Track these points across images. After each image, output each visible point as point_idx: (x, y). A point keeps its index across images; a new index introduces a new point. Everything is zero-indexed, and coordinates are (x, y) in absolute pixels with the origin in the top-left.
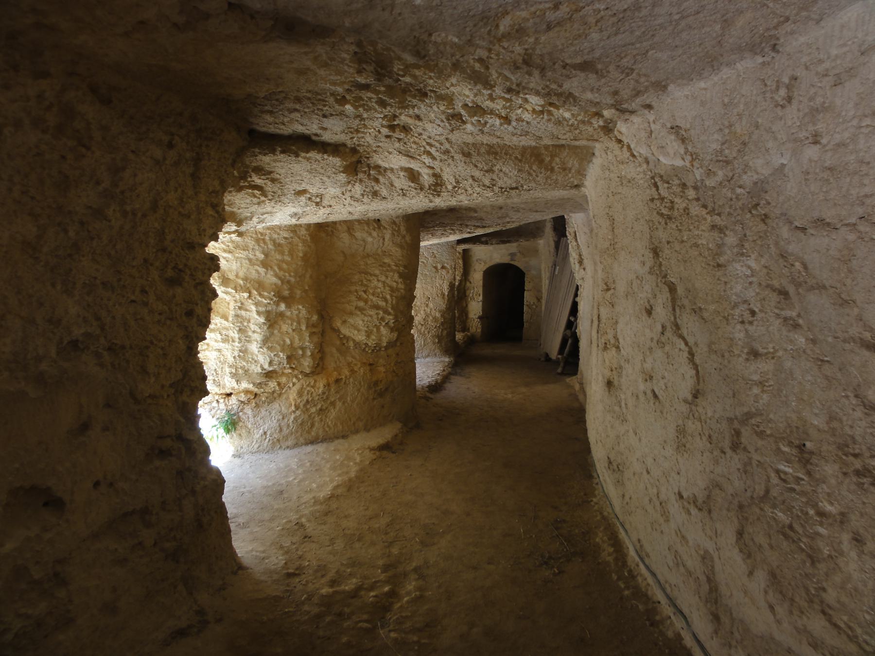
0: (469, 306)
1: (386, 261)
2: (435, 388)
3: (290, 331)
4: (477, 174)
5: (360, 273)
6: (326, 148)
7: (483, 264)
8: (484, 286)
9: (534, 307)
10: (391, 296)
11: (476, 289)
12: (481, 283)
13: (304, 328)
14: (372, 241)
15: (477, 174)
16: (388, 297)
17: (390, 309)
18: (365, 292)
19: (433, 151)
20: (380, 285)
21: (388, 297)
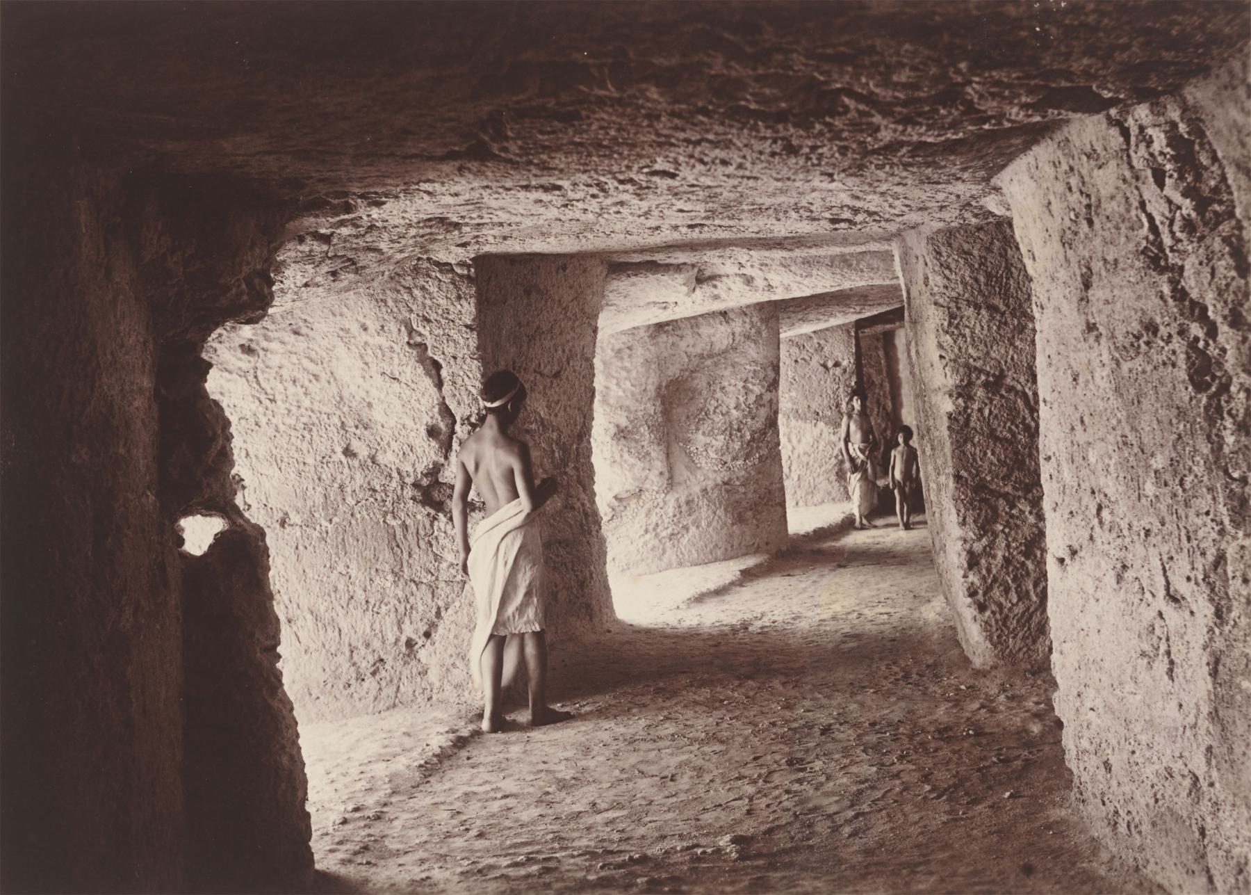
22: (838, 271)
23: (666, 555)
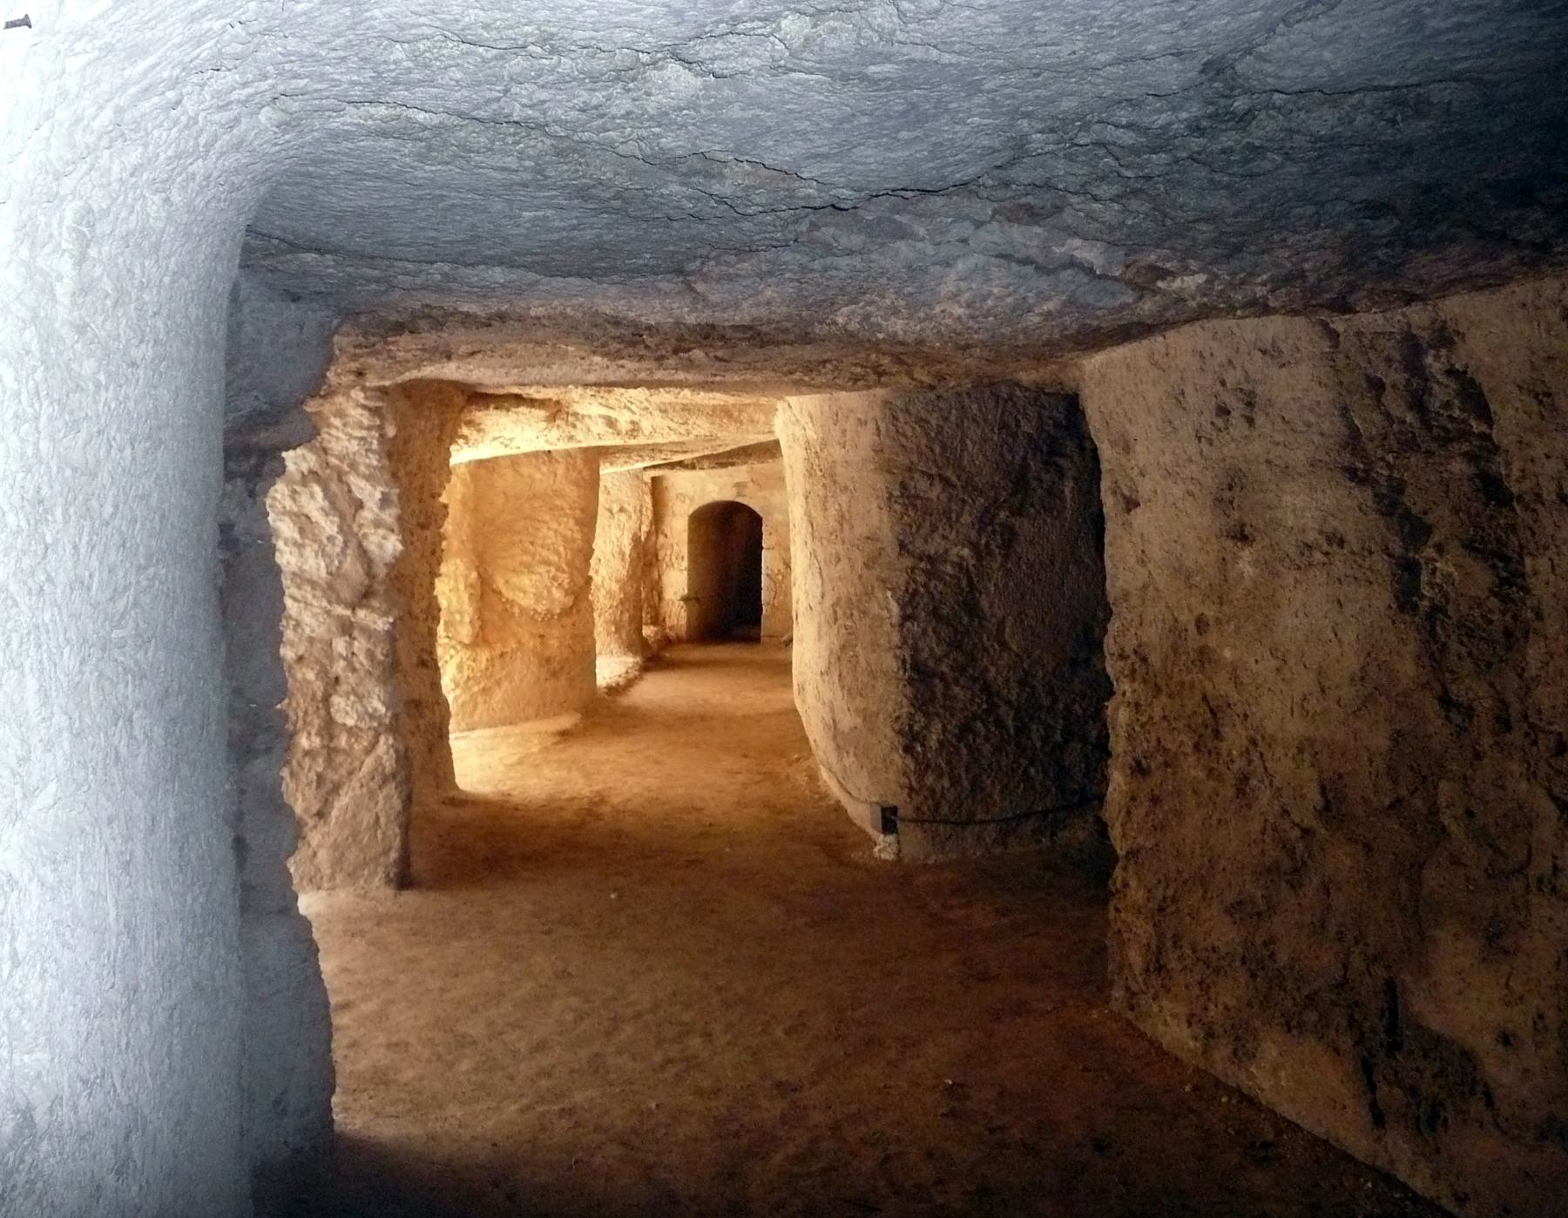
0: (664, 578)
1: (558, 502)
2: (615, 690)
3: (447, 592)
4: (673, 425)
5: (525, 518)
6: (532, 403)
7: (688, 502)
8: (691, 541)
9: (780, 577)
10: (565, 548)
11: (675, 547)
12: (685, 536)
13: (462, 587)
14: (540, 478)
15: (673, 425)
16: (561, 549)
17: (564, 566)
18: (532, 543)
19: (633, 407)
20: (551, 534)
21: (561, 549)
22: (718, 421)
23: (478, 712)
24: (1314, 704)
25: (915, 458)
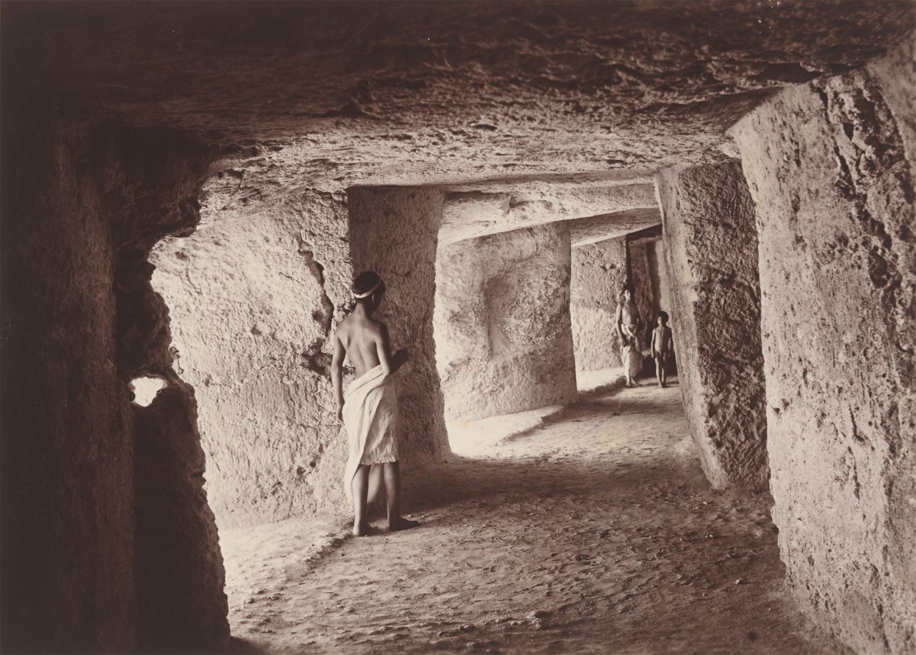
22: (614, 198)
24: (173, 349)
25: (703, 211)
